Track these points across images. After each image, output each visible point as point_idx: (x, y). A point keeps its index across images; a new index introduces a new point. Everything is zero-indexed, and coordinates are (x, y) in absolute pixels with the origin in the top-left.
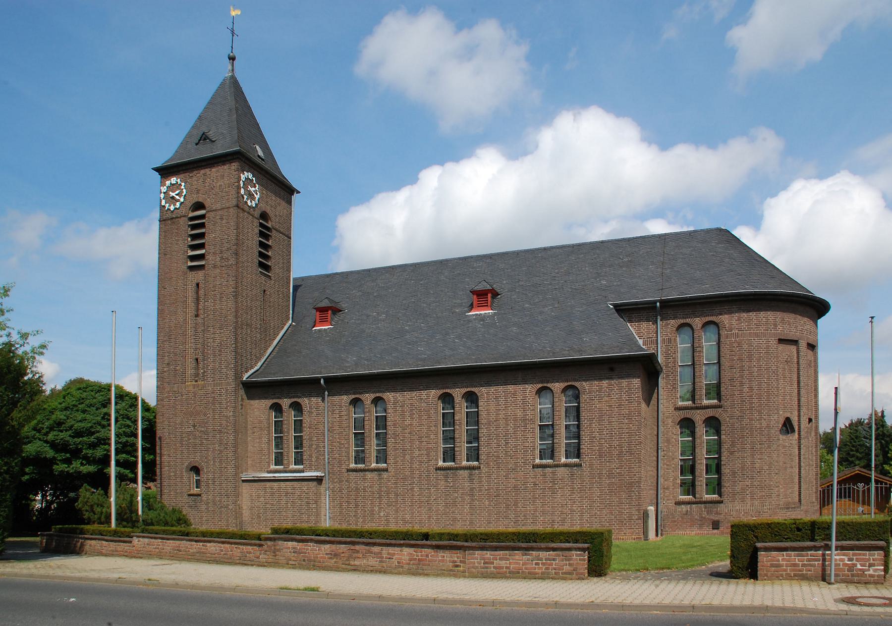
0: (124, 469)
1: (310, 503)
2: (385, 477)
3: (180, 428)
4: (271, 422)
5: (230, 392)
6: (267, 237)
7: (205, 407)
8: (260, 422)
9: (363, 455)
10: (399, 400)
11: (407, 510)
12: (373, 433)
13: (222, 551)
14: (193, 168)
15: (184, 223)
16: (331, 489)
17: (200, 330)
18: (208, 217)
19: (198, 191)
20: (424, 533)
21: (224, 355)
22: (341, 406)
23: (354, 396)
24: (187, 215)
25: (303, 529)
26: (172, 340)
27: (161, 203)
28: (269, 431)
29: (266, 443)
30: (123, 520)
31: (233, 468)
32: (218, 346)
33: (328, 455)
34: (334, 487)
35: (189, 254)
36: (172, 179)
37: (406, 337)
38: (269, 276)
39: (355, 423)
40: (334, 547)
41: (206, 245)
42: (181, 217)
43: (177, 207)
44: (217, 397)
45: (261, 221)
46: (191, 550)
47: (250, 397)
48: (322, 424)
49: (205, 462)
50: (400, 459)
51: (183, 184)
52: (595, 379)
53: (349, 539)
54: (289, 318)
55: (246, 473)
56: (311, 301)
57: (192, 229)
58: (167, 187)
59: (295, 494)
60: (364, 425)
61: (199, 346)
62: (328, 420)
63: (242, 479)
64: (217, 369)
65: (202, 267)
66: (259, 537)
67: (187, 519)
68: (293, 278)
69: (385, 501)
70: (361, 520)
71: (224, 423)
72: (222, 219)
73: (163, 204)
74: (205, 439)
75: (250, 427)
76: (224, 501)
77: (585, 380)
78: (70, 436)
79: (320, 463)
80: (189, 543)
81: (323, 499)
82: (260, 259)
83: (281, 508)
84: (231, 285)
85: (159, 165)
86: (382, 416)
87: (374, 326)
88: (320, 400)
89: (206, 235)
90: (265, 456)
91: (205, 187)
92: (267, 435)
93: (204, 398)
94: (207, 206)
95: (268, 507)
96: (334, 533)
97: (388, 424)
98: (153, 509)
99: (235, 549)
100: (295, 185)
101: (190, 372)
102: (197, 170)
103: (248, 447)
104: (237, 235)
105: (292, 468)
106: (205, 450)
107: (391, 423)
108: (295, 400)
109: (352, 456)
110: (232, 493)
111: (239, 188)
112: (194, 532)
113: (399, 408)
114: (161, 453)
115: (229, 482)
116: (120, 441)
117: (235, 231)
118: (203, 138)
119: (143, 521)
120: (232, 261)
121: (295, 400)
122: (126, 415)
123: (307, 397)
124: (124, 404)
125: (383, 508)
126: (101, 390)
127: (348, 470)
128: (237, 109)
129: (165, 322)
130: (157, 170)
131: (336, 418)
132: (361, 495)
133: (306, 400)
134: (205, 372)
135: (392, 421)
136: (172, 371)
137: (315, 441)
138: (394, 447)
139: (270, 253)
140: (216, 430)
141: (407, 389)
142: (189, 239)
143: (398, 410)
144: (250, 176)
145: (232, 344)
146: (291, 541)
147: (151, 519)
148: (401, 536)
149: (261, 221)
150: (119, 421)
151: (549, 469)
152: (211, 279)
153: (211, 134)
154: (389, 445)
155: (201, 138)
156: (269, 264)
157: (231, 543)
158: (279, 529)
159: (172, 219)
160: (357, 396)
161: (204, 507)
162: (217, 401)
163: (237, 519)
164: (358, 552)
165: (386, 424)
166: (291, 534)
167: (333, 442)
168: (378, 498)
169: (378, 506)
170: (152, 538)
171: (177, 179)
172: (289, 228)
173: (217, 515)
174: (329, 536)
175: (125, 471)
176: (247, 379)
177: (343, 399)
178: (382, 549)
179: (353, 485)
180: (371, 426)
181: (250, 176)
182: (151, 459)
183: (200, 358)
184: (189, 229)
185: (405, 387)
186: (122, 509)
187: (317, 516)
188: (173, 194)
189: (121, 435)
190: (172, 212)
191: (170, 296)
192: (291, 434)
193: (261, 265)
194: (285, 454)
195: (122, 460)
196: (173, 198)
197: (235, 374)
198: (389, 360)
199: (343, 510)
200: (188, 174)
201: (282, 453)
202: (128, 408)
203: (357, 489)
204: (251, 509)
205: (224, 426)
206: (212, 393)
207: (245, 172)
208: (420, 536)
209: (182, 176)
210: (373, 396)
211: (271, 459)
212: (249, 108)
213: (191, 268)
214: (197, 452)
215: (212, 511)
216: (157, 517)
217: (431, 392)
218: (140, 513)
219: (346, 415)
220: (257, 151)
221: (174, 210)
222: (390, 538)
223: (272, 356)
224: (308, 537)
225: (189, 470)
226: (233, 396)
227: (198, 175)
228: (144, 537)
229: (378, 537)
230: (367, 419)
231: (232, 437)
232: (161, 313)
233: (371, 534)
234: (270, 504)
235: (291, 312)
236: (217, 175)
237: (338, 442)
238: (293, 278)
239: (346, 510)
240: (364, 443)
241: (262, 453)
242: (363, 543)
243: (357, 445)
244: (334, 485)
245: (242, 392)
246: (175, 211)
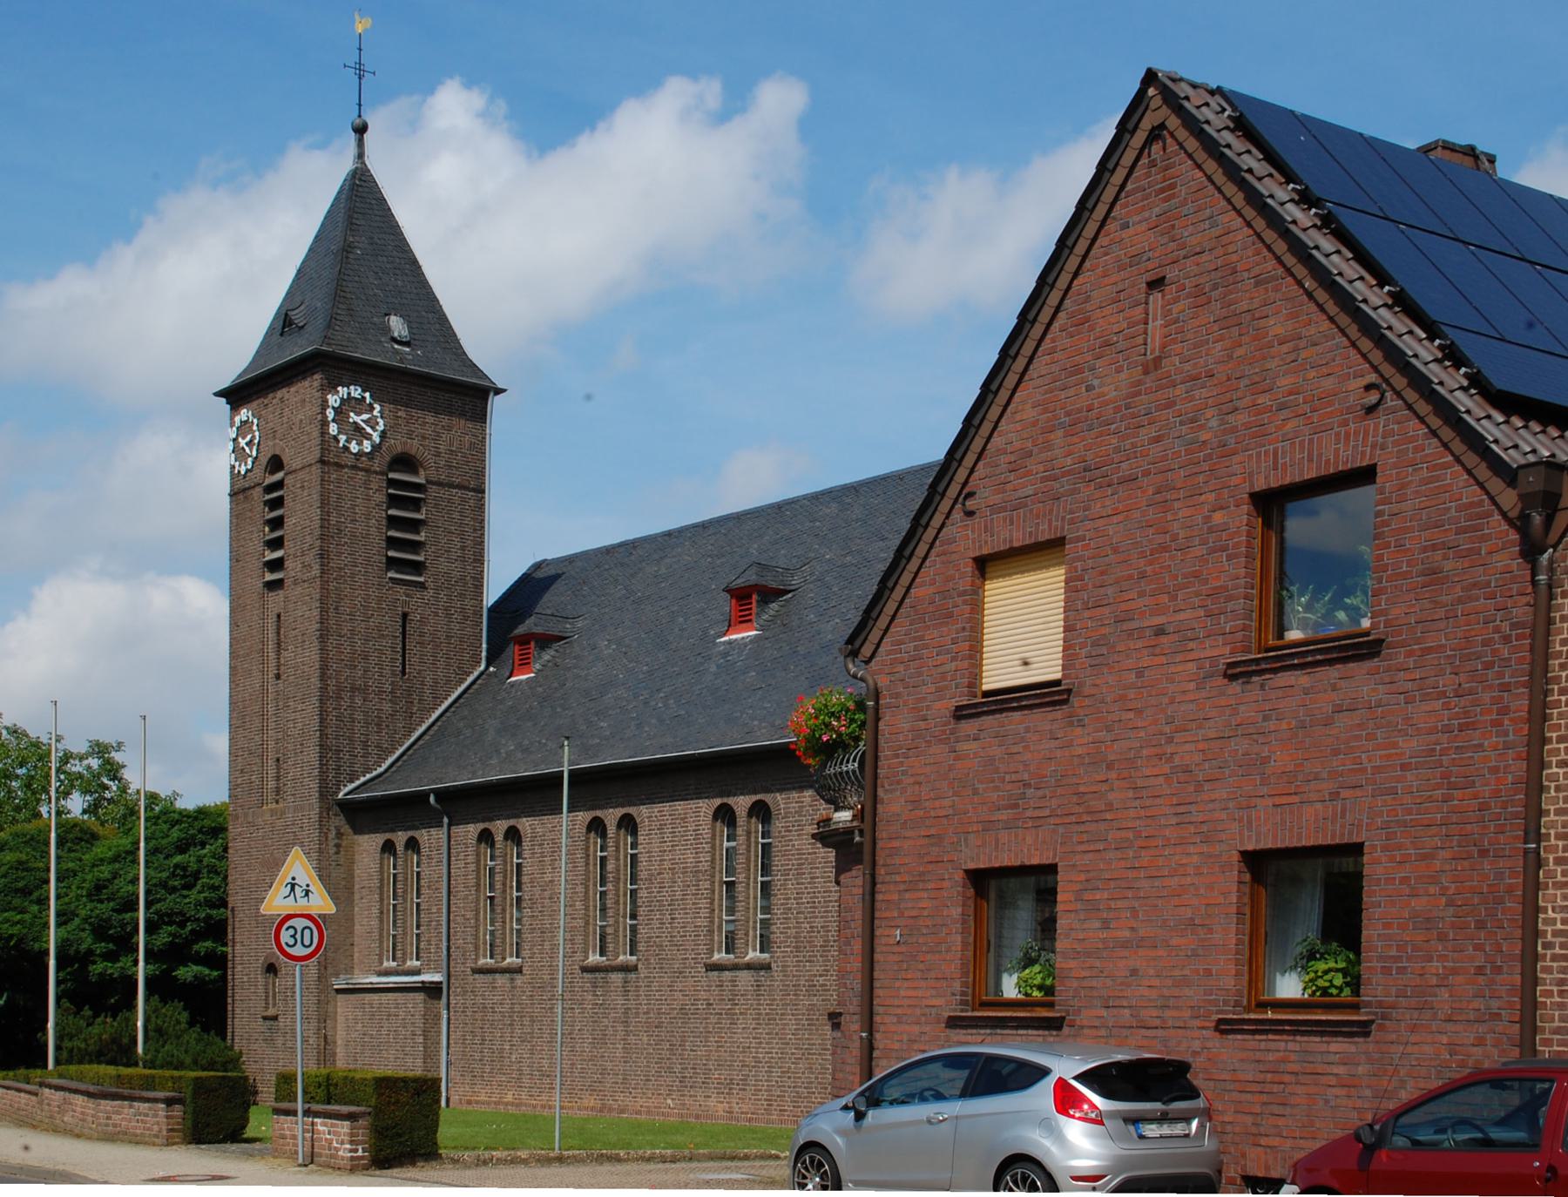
35: (266, 559)
42: (254, 487)
51: (255, 421)
52: (794, 789)
57: (271, 510)
63: (335, 987)
77: (781, 790)
78: (113, 910)
85: (226, 382)
105: (484, 964)
111: (324, 423)
130: (219, 394)
139: (423, 534)
142: (267, 529)
151: (727, 973)
176: (346, 795)
184: (267, 509)
189: (200, 905)
209: (255, 404)
217: (577, 816)
223: (421, 742)
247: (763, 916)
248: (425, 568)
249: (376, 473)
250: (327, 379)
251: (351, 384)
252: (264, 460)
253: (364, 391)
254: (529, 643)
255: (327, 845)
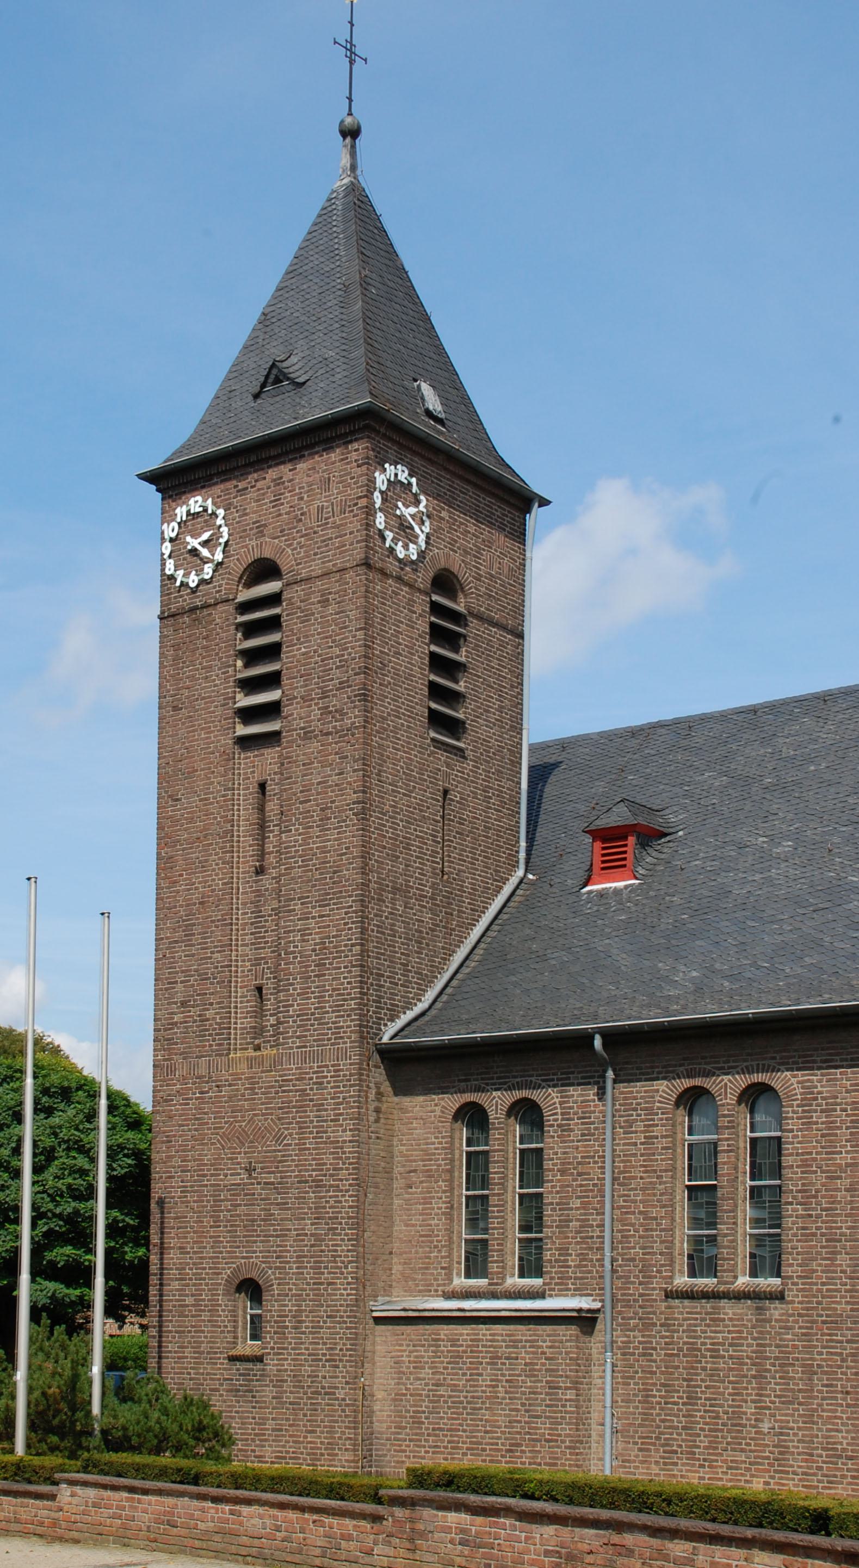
0: (68, 1286)
1: (559, 1388)
2: (776, 1314)
3: (212, 1175)
4: (457, 1156)
5: (344, 1075)
6: (452, 640)
7: (279, 1119)
8: (428, 1156)
9: (714, 1251)
10: (819, 1093)
11: (841, 1418)
12: (741, 1189)
13: (278, 1529)
14: (246, 466)
15: (225, 617)
16: (619, 1348)
17: (267, 909)
18: (290, 599)
19: (260, 530)
20: (815, 1510)
21: (330, 975)
22: (650, 1111)
23: (687, 1083)
24: (231, 597)
25: (491, 1477)
26: (197, 939)
27: (163, 570)
28: (451, 1181)
29: (443, 1213)
30: (51, 1430)
31: (348, 1283)
32: (314, 950)
33: (613, 1249)
34: (629, 1342)
36: (192, 501)
37: (851, 906)
38: (461, 750)
39: (690, 1158)
40: (566, 1532)
41: (284, 678)
42: (216, 604)
43: (207, 577)
44: (311, 1089)
45: (435, 598)
46: (201, 1526)
47: (402, 1088)
48: (595, 1162)
49: (277, 1268)
50: (820, 1265)
51: (221, 512)
53: (605, 1514)
54: (517, 862)
55: (387, 1299)
56: (582, 808)
57: (247, 636)
58: (179, 524)
59: (517, 1358)
60: (716, 1165)
61: (267, 952)
62: (614, 1150)
63: (375, 1314)
64: (313, 1014)
65: (272, 738)
66: (377, 1494)
67: (222, 1427)
68: (530, 745)
69: (774, 1386)
70: (703, 1441)
71: (329, 1159)
72: (325, 602)
73: (168, 572)
74: (278, 1204)
75: (402, 1170)
76: (325, 1377)
79: (590, 1272)
80: (195, 1503)
81: (596, 1375)
82: (434, 706)
83: (478, 1398)
84: (349, 783)
85: (154, 463)
86: (770, 1138)
87: (757, 877)
88: (592, 1093)
89: (284, 649)
90: (440, 1251)
91: (280, 515)
92: (444, 1192)
93: (277, 1093)
94: (284, 569)
95: (443, 1396)
96: (569, 1492)
97: (787, 1161)
98: (132, 1399)
99: (312, 1526)
100: (536, 486)
101: (242, 1022)
102: (255, 471)
103: (392, 1226)
104: (366, 646)
106: (277, 1236)
107: (795, 1161)
108: (525, 1093)
109: (681, 1254)
110: (344, 1355)
111: (370, 511)
112: (211, 1473)
113: (818, 1117)
114: (162, 1243)
115: (339, 1323)
116: (58, 1211)
117: (360, 634)
118: (272, 377)
119: (104, 1432)
120: (354, 717)
121: (525, 1093)
122: (76, 1142)
123: (554, 1086)
124: (71, 1112)
125: (769, 1408)
126: (12, 1077)
127: (670, 1295)
128: (365, 284)
129: (178, 892)
130: (151, 478)
131: (635, 1144)
132: (704, 1369)
133: (553, 1095)
134: (279, 1023)
135: (797, 1154)
136: (195, 1021)
137: (577, 1209)
138: (803, 1228)
139: (462, 683)
140: (307, 1182)
141: (842, 1060)
142: (239, 663)
143: (817, 1123)
144: (403, 476)
145: (353, 945)
146: (456, 1511)
147: (125, 1428)
148: (751, 1515)
149: (435, 598)
150: (56, 1158)
152: (297, 770)
153: (295, 366)
154: (788, 1222)
155: (267, 377)
156: (461, 716)
157: (303, 1509)
158: (429, 1473)
159: (193, 610)
160: (697, 1082)
161: (268, 1393)
162: (311, 1100)
163: (355, 1428)
164: (630, 1553)
165: (780, 1161)
166: (458, 1489)
167: (627, 1213)
168: (754, 1377)
169: (753, 1401)
170: (105, 1487)
171: (205, 500)
172: (519, 610)
173: (305, 1415)
174: (557, 1500)
175: (67, 1291)
176: (391, 1039)
177: (657, 1091)
178: (694, 1548)
179: (682, 1338)
180: (736, 1168)
181: (403, 476)
182: (140, 1258)
183: (269, 986)
184: (239, 635)
185: (837, 1054)
186: (47, 1400)
187: (577, 1424)
188: (193, 543)
189: (62, 1196)
190: (194, 591)
191: (191, 820)
192: (510, 1189)
193: (436, 719)
194: (493, 1245)
195: (62, 1263)
196: (194, 552)
197: (360, 1026)
198: (794, 977)
199: (654, 1408)
200: (235, 482)
201: (484, 1242)
202: (81, 1122)
203: (693, 1348)
204: (397, 1399)
205: (328, 1170)
206: (297, 1079)
207: (387, 465)
208: (806, 1518)
209: (217, 490)
210: (742, 1081)
211: (456, 1259)
212: (401, 273)
213: (245, 742)
214: (255, 1242)
215: (290, 1403)
216: (138, 1423)
218: (96, 1409)
219: (666, 1137)
220: (423, 398)
221: (198, 586)
222: (721, 1516)
223: (465, 970)
224: (500, 1500)
225: (233, 1290)
226: (351, 1086)
227: (259, 485)
228: (85, 1484)
229: (689, 1512)
230: (723, 1146)
231: (350, 1201)
232: (165, 865)
233: (669, 1502)
234: (449, 1385)
235: (523, 844)
236: (311, 479)
237: (640, 1213)
238: (530, 745)
239: (661, 1409)
240: (714, 1215)
241: (432, 1242)
242: (644, 1529)
243: (695, 1222)
244: (628, 1336)
245: (379, 1075)
246: (201, 588)
247: (521, 1236)
248: (465, 730)
249: (419, 590)
250: (373, 450)
251: (398, 463)
252: (237, 567)
253: (411, 475)
254: (626, 838)
255: (367, 1109)
